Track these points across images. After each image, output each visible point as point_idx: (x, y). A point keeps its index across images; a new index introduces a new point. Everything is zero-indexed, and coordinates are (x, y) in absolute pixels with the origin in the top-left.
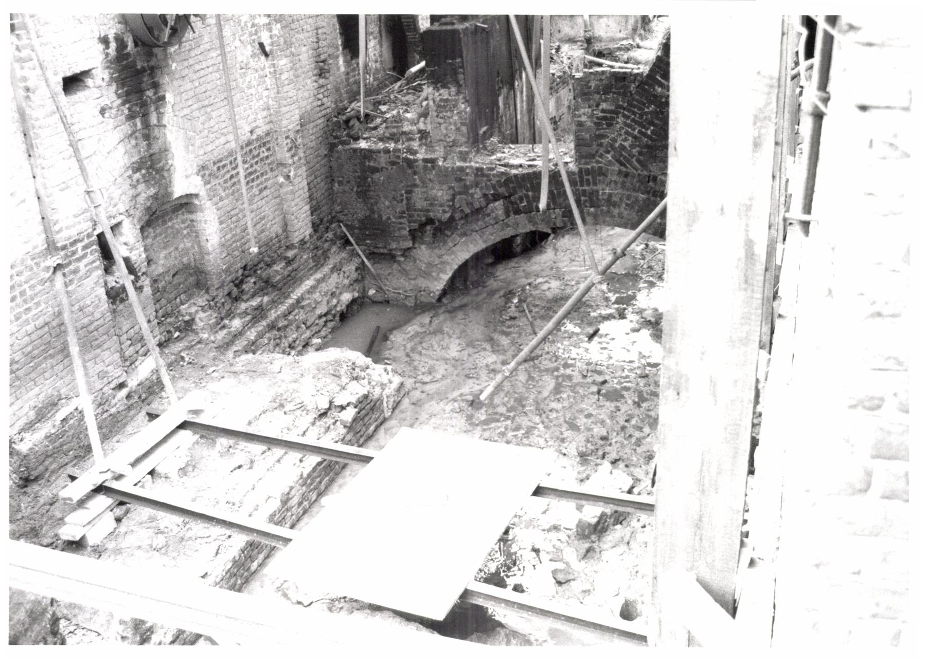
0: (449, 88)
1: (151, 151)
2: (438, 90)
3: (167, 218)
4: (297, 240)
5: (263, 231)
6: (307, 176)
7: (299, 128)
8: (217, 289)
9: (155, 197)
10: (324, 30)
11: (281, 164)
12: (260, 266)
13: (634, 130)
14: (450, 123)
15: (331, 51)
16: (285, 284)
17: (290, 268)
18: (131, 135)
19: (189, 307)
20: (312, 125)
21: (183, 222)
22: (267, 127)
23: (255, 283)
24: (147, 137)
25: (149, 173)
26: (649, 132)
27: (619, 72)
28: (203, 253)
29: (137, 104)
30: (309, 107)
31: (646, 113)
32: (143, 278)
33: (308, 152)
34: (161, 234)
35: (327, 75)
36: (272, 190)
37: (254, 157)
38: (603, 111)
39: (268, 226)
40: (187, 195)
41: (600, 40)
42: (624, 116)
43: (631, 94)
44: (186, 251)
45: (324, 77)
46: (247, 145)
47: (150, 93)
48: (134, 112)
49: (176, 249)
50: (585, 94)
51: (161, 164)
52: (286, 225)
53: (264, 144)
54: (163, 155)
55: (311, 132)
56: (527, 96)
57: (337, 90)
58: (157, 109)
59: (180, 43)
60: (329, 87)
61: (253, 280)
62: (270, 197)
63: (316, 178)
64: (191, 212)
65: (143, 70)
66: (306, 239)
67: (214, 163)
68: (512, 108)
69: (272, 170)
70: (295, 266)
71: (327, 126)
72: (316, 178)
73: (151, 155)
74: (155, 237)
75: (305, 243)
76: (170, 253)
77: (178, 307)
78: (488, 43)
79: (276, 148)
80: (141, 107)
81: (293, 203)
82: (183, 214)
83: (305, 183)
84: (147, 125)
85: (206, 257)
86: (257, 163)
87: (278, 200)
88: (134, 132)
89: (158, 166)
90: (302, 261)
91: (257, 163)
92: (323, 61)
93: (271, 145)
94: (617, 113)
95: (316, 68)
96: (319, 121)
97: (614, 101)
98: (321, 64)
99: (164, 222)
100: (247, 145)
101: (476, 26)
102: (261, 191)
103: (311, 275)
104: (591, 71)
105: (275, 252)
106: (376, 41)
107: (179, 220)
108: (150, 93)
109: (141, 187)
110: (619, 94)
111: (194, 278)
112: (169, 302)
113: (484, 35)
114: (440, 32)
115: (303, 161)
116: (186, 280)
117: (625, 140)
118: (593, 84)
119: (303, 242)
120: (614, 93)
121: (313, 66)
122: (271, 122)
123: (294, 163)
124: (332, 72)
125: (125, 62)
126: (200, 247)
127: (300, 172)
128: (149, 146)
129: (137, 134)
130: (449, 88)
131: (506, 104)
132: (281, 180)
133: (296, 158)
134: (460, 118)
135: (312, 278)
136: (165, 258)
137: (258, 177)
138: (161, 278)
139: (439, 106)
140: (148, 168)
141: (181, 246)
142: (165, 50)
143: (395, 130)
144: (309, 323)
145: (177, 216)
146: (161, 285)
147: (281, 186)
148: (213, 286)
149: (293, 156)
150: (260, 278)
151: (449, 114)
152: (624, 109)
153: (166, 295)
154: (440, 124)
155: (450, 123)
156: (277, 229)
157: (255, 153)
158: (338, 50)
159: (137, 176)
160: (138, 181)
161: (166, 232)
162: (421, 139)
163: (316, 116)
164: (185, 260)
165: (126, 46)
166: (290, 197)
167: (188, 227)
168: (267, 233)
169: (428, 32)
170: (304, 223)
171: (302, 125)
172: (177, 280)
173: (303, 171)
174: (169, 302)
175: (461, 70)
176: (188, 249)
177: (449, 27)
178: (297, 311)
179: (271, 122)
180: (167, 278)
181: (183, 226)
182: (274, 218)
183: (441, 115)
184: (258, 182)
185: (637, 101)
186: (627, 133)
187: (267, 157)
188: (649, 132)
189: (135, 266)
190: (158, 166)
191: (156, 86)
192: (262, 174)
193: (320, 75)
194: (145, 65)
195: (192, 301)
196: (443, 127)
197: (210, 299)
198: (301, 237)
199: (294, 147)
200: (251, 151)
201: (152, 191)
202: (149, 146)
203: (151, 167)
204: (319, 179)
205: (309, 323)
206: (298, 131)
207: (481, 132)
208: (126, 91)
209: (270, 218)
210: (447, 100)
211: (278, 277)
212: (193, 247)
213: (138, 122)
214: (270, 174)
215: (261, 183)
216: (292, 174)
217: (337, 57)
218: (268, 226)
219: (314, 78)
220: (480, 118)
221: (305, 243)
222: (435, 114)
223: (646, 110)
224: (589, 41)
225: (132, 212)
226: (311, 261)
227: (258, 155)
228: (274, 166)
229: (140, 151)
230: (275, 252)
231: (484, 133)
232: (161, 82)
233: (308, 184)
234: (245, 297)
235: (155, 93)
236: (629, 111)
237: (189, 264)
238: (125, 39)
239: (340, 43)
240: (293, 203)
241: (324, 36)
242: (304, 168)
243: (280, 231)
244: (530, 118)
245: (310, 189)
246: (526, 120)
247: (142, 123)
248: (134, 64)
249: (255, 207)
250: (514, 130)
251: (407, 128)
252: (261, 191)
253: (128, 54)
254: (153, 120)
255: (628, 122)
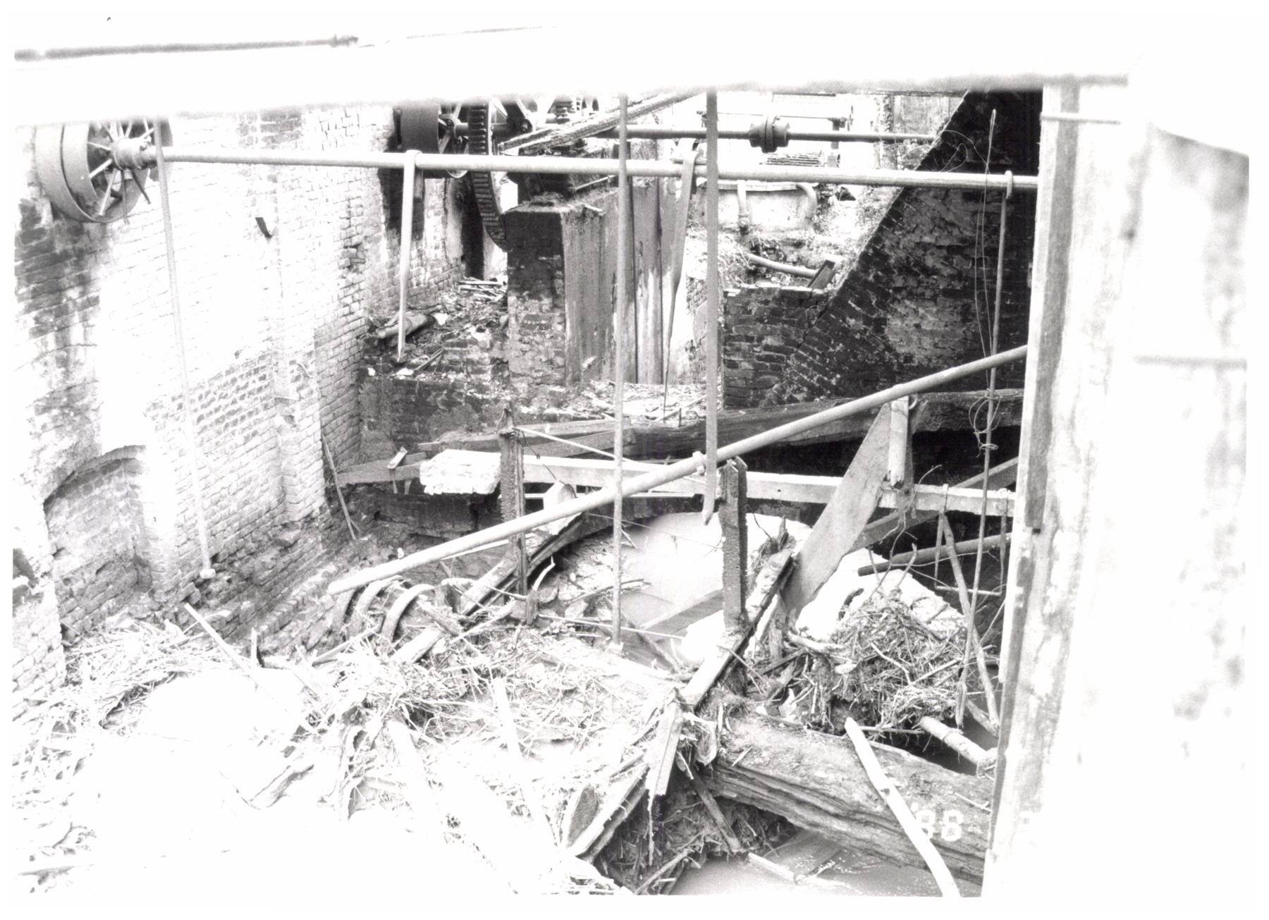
0: (540, 299)
1: (69, 383)
2: (524, 301)
3: (92, 482)
4: (301, 515)
5: (246, 503)
6: (322, 416)
7: (312, 348)
8: (168, 593)
9: (72, 452)
10: (359, 202)
11: (281, 401)
12: (239, 555)
13: (811, 377)
14: (539, 352)
15: (368, 231)
16: (275, 583)
17: (287, 558)
18: (37, 359)
19: (120, 620)
20: (334, 343)
21: (119, 489)
22: (264, 347)
23: (229, 581)
24: (64, 362)
25: (63, 414)
26: (834, 382)
27: (793, 292)
28: (147, 538)
29: (50, 311)
30: (329, 319)
31: (831, 356)
32: (42, 581)
33: (325, 382)
34: (80, 509)
35: (361, 267)
36: (265, 437)
37: (238, 389)
38: (767, 348)
39: (256, 494)
40: (126, 448)
41: (757, 228)
42: (799, 357)
43: (810, 326)
44: (121, 533)
45: (356, 271)
46: (228, 373)
47: (73, 293)
48: (45, 324)
49: (106, 530)
50: (742, 322)
51: (85, 401)
52: (284, 492)
53: (256, 371)
54: (89, 387)
55: (331, 353)
56: (655, 312)
57: (375, 291)
58: (84, 319)
59: (125, 217)
60: (362, 285)
61: (226, 578)
62: (261, 448)
63: (335, 417)
64: (133, 472)
65: (65, 255)
66: (314, 515)
67: (173, 399)
68: (632, 329)
69: (266, 407)
70: (295, 554)
71: (357, 344)
72: (335, 417)
73: (69, 388)
74: (71, 514)
75: (313, 519)
76: (95, 537)
77: (102, 618)
78: (601, 233)
79: (275, 376)
80: (57, 316)
81: (297, 459)
82: (119, 475)
83: (318, 425)
84: (64, 344)
85: (152, 543)
86: (242, 398)
87: (273, 452)
88: (43, 355)
89: (79, 404)
90: (307, 547)
91: (242, 398)
92: (356, 246)
93: (267, 372)
94: (788, 353)
95: (343, 256)
96: (345, 338)
97: (785, 335)
98: (353, 250)
99: (88, 489)
100: (228, 373)
101: (585, 209)
102: (247, 439)
103: (320, 567)
104: (752, 286)
105: (265, 533)
106: (439, 218)
107: (112, 486)
108: (73, 293)
109: (51, 436)
110: (791, 324)
111: (132, 575)
112: (87, 613)
113: (597, 220)
114: (534, 215)
115: (316, 395)
116: (119, 576)
117: (799, 390)
118: (754, 308)
119: (309, 519)
120: (785, 322)
121: (339, 253)
122: (269, 339)
123: (301, 398)
124: (368, 263)
125: (34, 243)
126: (143, 527)
127: (309, 411)
128: (67, 374)
129: (48, 358)
130: (540, 299)
131: (625, 323)
132: (279, 421)
133: (304, 392)
134: (555, 345)
135: (321, 571)
136: (87, 544)
137: (243, 418)
138: (78, 575)
139: (524, 326)
140: (62, 407)
141: (114, 526)
142: (104, 225)
143: (457, 357)
144: (311, 642)
145: (109, 479)
146: (76, 587)
147: (279, 430)
148: (161, 587)
149: (299, 389)
150: (240, 574)
151: (538, 338)
152: (799, 346)
153: (85, 602)
154: (524, 352)
155: (539, 352)
156: (270, 498)
157: (241, 383)
158: (379, 230)
159: (45, 418)
160: (44, 427)
161: (90, 504)
162: (495, 371)
163: (340, 331)
164: (119, 548)
165: (38, 219)
166: (295, 448)
167: (127, 495)
168: (254, 505)
169: (512, 215)
170: (311, 490)
171: (317, 344)
172: (103, 577)
173: (315, 409)
174: (87, 613)
175: (559, 273)
176: (124, 531)
177: (545, 209)
178: (293, 624)
179: (269, 339)
180: (87, 576)
181: (118, 494)
182: (267, 482)
183: (526, 339)
184: (245, 424)
185: (818, 335)
186: (801, 381)
187: (260, 389)
188: (834, 382)
189: (31, 563)
190: (79, 404)
191: (84, 282)
192: (250, 414)
193: (350, 267)
194: (70, 247)
195: (126, 610)
196: (529, 355)
197: (156, 606)
198: (307, 512)
199: (302, 376)
200: (234, 380)
201: (67, 443)
202: (67, 374)
203: (67, 406)
204: (339, 420)
205: (311, 642)
206: (310, 354)
207: (585, 365)
208: (34, 290)
209: (260, 481)
210: (535, 318)
211: (267, 573)
212: (132, 526)
213: (50, 337)
214: (262, 414)
215: (249, 427)
216: (297, 415)
217: (377, 240)
218: (256, 494)
219: (341, 272)
220: (584, 346)
221: (313, 519)
222: (518, 337)
223: (831, 350)
224: (744, 230)
225: (30, 476)
226: (321, 546)
227: (246, 386)
228: (270, 402)
229: (50, 383)
230: (265, 533)
231: (589, 366)
232: (93, 275)
233: (322, 427)
234: (212, 602)
235: (83, 294)
236: (805, 350)
237: (125, 553)
238: (38, 208)
239: (383, 219)
240: (297, 459)
241: (360, 210)
242: (317, 405)
243: (274, 502)
244: (656, 346)
245: (324, 434)
246: (651, 345)
247: (57, 341)
248: (51, 245)
249: (236, 464)
250: (633, 360)
251: (475, 355)
252: (247, 439)
253: (42, 231)
254: (76, 333)
255: (804, 365)
